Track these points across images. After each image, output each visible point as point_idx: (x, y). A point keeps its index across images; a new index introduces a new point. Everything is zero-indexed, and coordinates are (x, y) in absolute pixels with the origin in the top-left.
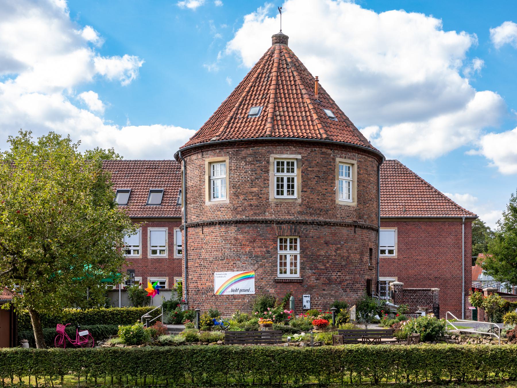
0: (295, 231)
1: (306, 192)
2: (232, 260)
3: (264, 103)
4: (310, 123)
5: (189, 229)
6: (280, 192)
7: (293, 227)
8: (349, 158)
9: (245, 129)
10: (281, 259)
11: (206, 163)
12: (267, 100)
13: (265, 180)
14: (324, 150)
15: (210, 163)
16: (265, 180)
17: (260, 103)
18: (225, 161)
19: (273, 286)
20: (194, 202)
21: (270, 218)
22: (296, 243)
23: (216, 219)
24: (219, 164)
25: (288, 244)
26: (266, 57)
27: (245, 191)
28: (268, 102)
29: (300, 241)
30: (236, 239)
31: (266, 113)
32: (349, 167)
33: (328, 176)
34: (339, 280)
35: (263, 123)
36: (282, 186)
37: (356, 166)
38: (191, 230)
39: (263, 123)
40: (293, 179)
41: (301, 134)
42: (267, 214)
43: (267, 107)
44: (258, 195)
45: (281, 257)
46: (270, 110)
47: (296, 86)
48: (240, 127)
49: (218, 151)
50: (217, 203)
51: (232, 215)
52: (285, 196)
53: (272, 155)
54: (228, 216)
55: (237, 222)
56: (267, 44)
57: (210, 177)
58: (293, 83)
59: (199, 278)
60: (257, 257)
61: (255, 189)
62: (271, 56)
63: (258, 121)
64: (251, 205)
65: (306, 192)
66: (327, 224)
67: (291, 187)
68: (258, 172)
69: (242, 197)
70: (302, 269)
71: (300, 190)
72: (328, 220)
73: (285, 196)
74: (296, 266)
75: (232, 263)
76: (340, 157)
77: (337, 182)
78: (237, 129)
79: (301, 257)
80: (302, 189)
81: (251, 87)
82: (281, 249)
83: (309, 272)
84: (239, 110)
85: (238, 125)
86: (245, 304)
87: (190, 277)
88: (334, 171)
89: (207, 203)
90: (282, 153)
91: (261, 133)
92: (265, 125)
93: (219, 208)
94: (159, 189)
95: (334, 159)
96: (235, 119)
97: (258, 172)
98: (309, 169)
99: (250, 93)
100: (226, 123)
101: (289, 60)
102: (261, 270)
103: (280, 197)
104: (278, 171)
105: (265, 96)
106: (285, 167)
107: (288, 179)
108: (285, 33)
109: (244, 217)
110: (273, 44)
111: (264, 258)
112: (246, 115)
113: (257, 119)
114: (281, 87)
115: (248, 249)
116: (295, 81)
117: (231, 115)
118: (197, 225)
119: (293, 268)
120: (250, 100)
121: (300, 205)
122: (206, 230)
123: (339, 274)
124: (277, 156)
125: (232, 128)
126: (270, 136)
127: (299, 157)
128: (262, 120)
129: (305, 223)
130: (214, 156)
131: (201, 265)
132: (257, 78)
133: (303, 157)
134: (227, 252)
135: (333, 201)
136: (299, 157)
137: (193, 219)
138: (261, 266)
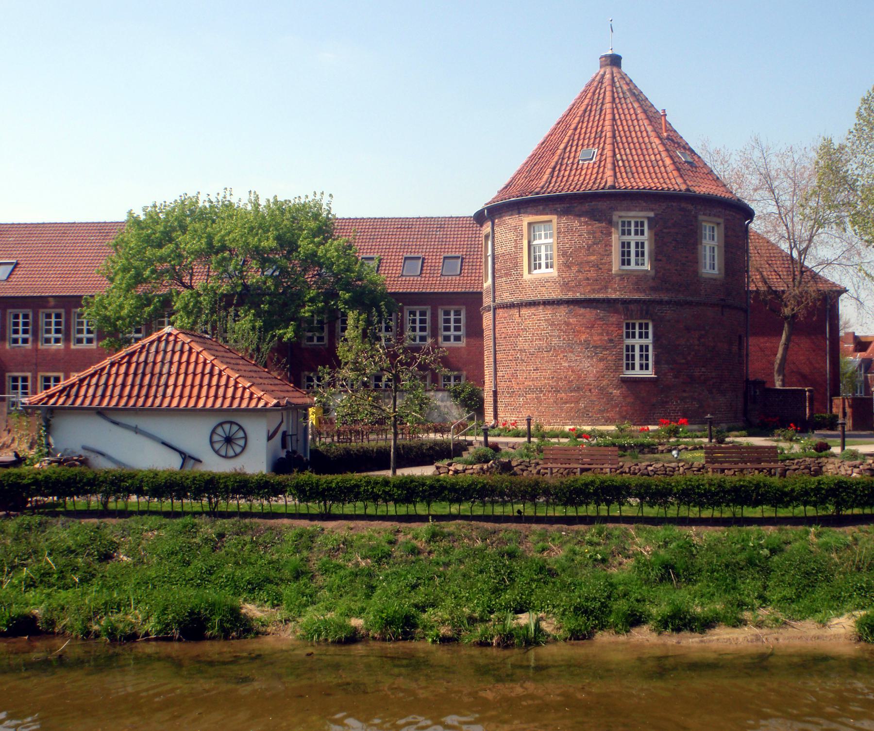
0: (647, 313)
1: (660, 260)
2: (562, 352)
3: (599, 144)
4: (662, 169)
5: (498, 311)
6: (625, 262)
7: (644, 308)
8: (715, 216)
9: (577, 178)
10: (628, 350)
11: (525, 224)
12: (603, 139)
13: (606, 246)
14: (683, 205)
15: (530, 224)
16: (606, 246)
17: (594, 144)
18: (551, 221)
19: (617, 387)
20: (506, 275)
21: (613, 296)
22: (647, 328)
23: (539, 297)
24: (542, 226)
25: (637, 331)
26: (595, 84)
27: (579, 260)
28: (605, 143)
29: (654, 327)
30: (568, 324)
31: (604, 157)
32: (713, 228)
33: (691, 240)
34: (702, 378)
35: (601, 170)
36: (629, 253)
37: (722, 226)
38: (500, 312)
39: (601, 170)
40: (643, 244)
41: (647, 185)
42: (610, 290)
43: (603, 149)
44: (597, 267)
45: (627, 347)
46: (608, 152)
47: (638, 121)
48: (569, 176)
49: (541, 208)
50: (540, 277)
51: (562, 291)
52: (633, 266)
53: (616, 213)
54: (555, 295)
55: (569, 302)
56: (592, 69)
57: (529, 242)
58: (634, 117)
59: (514, 375)
60: (596, 347)
61: (592, 258)
62: (601, 82)
63: (593, 168)
64: (588, 279)
65: (660, 260)
66: (689, 304)
67: (640, 254)
68: (597, 235)
69: (575, 269)
70: (657, 363)
71: (653, 259)
72: (689, 299)
73: (633, 266)
74: (647, 359)
75: (562, 355)
76: (704, 214)
77: (699, 247)
78: (565, 179)
79: (654, 347)
80: (656, 256)
81: (579, 123)
82: (628, 337)
83: (665, 367)
84: (565, 153)
85: (567, 173)
86: (579, 410)
87: (499, 374)
88: (696, 233)
89: (526, 276)
90: (630, 210)
91: (600, 183)
92: (603, 173)
93: (543, 282)
94: (416, 255)
95: (696, 217)
96: (561, 165)
97: (597, 235)
98: (665, 230)
99: (578, 131)
100: (549, 170)
101: (625, 88)
102: (601, 365)
103: (626, 267)
104: (623, 233)
105: (599, 135)
106: (633, 228)
107: (637, 244)
108: (616, 52)
109: (578, 294)
110: (601, 67)
111: (605, 349)
112: (576, 160)
113: (591, 166)
114: (619, 123)
115: (583, 338)
116: (636, 115)
117: (555, 160)
118: (512, 306)
119: (644, 362)
120: (579, 140)
121: (653, 279)
122: (525, 312)
123: (703, 370)
124: (623, 214)
125: (558, 177)
126: (614, 187)
127: (652, 214)
128: (599, 167)
129: (660, 302)
130: (536, 214)
131: (516, 359)
132: (585, 111)
133: (656, 215)
134: (555, 341)
135: (696, 272)
136: (652, 214)
137: (506, 297)
138: (601, 360)
